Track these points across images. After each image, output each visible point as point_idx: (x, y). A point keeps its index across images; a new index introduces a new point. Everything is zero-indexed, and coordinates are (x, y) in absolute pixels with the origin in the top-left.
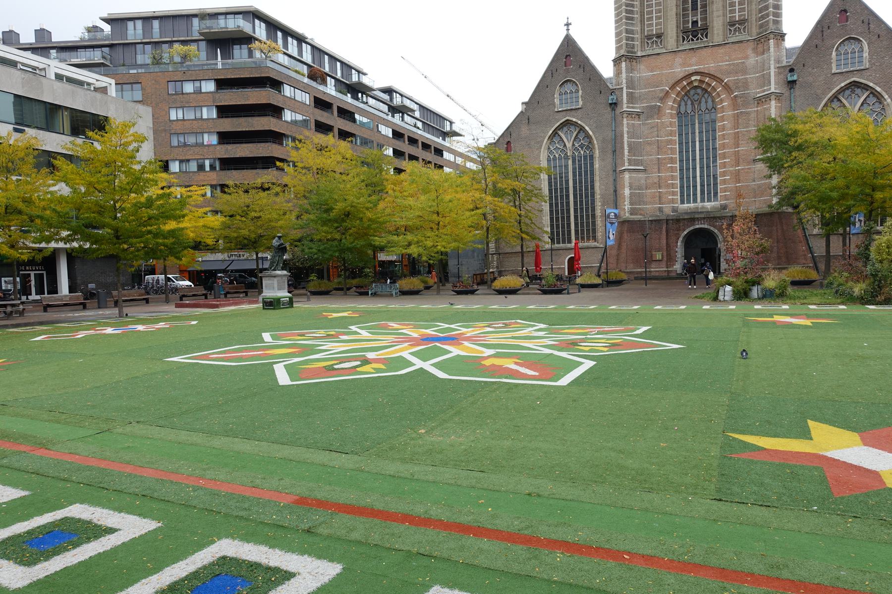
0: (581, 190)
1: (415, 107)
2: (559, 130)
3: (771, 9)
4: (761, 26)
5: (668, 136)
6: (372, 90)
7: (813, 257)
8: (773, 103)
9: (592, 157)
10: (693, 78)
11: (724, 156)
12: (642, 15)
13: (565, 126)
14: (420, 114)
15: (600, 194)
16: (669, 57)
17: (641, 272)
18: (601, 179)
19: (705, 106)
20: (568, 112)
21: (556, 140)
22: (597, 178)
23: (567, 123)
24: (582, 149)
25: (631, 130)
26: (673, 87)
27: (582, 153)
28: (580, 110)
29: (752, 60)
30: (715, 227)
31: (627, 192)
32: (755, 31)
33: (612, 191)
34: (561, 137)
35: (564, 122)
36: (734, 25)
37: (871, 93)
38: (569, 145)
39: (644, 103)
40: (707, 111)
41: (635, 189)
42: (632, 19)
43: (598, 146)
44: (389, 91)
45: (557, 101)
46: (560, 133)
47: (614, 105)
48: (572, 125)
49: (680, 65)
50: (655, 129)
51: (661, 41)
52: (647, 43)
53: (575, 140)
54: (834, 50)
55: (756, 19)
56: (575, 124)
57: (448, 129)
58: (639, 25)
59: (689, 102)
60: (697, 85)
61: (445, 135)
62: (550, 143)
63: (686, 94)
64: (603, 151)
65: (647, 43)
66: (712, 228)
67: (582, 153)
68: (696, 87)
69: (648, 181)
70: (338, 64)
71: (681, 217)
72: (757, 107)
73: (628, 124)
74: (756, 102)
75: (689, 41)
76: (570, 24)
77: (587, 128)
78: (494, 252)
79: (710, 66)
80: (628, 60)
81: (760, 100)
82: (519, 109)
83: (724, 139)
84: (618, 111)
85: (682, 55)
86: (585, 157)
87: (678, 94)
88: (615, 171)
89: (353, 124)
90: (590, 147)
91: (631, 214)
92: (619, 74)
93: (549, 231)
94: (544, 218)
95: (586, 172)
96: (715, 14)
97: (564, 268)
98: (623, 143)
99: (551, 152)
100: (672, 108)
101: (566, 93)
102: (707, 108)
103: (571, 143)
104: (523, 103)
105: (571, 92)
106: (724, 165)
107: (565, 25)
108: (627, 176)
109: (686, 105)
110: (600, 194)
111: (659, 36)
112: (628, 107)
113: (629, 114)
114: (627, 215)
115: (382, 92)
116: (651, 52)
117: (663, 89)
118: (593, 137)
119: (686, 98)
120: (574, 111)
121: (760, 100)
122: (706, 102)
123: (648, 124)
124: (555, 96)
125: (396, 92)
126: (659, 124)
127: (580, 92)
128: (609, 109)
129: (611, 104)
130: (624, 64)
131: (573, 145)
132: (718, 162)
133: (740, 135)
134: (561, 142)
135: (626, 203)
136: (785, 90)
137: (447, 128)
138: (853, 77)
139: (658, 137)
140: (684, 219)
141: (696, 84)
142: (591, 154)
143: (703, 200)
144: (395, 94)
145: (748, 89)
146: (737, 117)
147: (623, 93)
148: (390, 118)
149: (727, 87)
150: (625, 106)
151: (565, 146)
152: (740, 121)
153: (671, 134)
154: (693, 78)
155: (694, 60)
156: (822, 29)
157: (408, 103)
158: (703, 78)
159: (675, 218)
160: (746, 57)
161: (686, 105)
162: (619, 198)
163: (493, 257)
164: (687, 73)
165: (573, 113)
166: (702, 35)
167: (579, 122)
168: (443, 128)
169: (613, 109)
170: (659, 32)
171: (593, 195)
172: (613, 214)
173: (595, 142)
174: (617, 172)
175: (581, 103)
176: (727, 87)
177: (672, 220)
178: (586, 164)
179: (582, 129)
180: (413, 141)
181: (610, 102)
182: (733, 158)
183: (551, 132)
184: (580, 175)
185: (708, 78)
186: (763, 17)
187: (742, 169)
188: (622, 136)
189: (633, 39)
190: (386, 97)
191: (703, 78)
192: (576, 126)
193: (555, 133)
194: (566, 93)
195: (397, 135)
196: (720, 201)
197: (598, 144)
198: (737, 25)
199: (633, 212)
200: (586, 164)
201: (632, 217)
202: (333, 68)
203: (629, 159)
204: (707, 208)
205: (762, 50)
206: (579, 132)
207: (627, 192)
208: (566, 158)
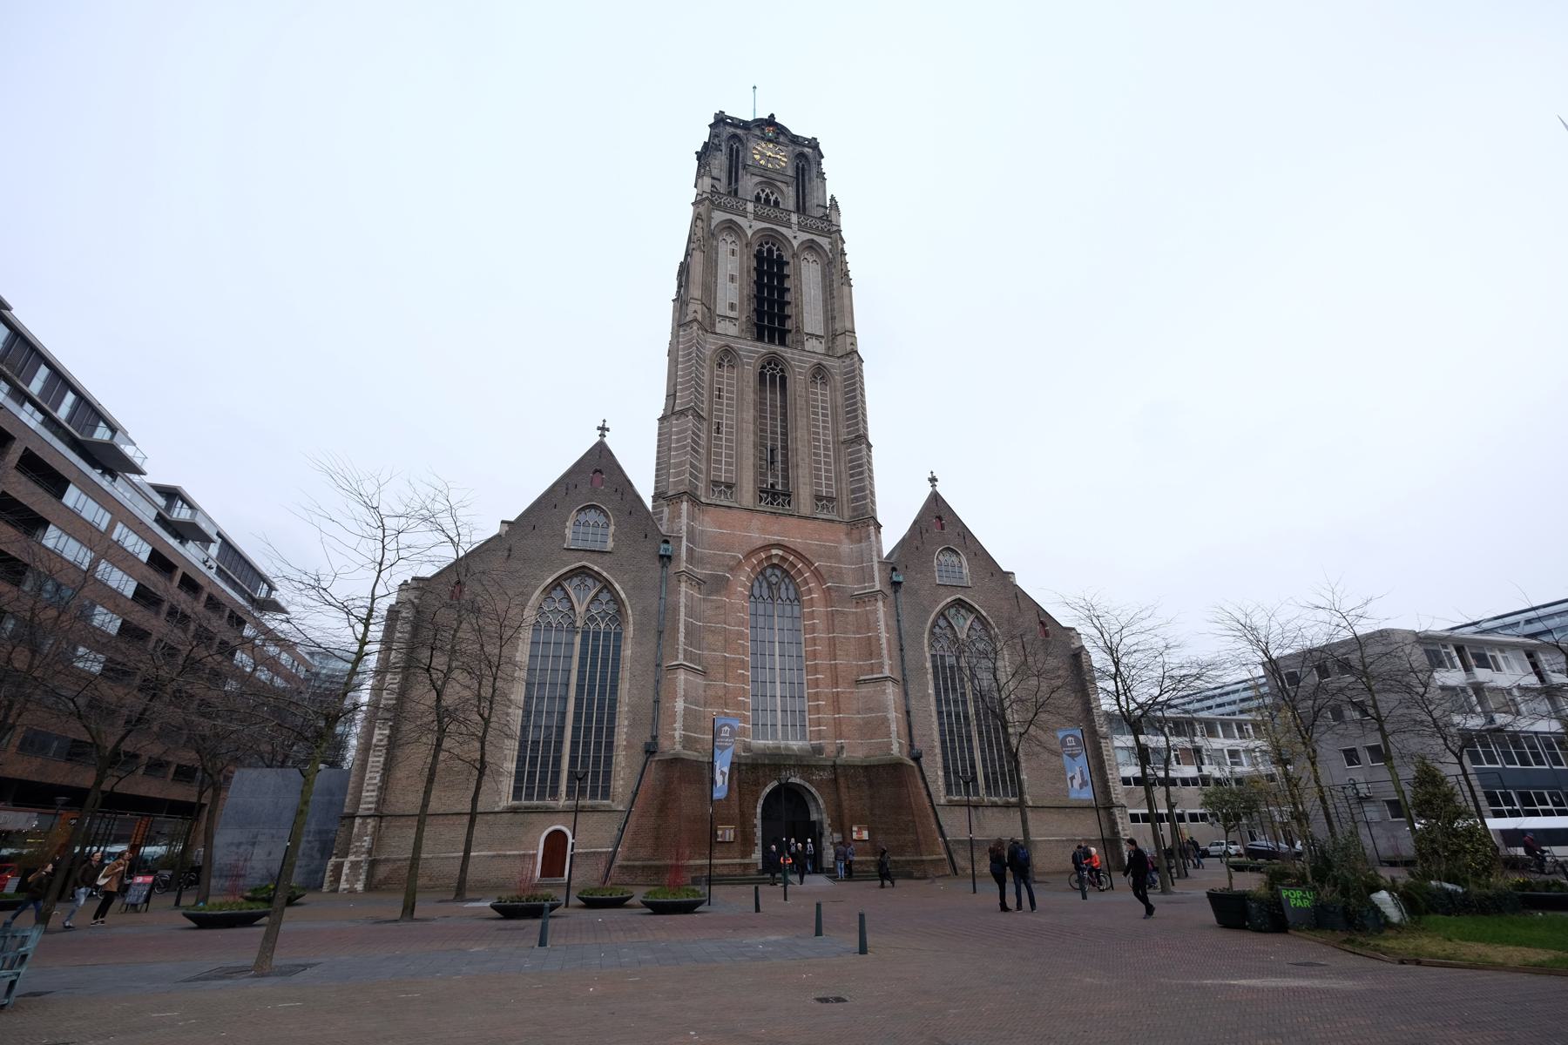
0: (591, 692)
2: (565, 580)
4: (855, 509)
5: (739, 626)
7: (946, 842)
9: (618, 636)
10: (774, 552)
13: (576, 576)
14: (219, 554)
15: (628, 705)
16: (745, 515)
17: (701, 867)
18: (633, 676)
19: (785, 594)
20: (588, 554)
21: (558, 594)
22: (625, 675)
23: (583, 572)
24: (603, 620)
25: (690, 604)
26: (748, 556)
27: (602, 626)
28: (606, 557)
29: (846, 547)
30: (811, 782)
31: (680, 705)
32: (847, 514)
33: (651, 701)
34: (566, 593)
35: (576, 569)
36: (821, 500)
37: (977, 617)
39: (707, 569)
40: (788, 602)
41: (691, 703)
43: (634, 619)
44: (172, 494)
45: (569, 533)
46: (566, 585)
47: (666, 559)
48: (590, 576)
50: (722, 611)
51: (732, 493)
52: (713, 490)
53: (592, 602)
55: (848, 501)
56: (596, 576)
57: (263, 595)
59: (765, 585)
60: (777, 562)
62: (545, 600)
63: (761, 572)
64: (640, 628)
65: (713, 490)
66: (807, 785)
67: (602, 626)
68: (774, 566)
69: (709, 692)
71: (760, 761)
72: (856, 607)
74: (854, 601)
75: (767, 504)
77: (617, 586)
78: (372, 812)
79: (795, 540)
80: (690, 502)
81: (860, 598)
82: (494, 529)
83: (815, 645)
84: (672, 569)
85: (761, 517)
86: (607, 635)
87: (753, 569)
88: (658, 665)
89: (54, 500)
90: (619, 615)
91: (684, 747)
92: (674, 518)
93: (514, 771)
95: (605, 661)
96: (801, 480)
97: (535, 856)
98: (676, 621)
100: (744, 586)
101: (586, 524)
102: (788, 598)
104: (503, 522)
105: (596, 525)
107: (599, 428)
108: (682, 676)
109: (761, 587)
110: (628, 705)
111: (729, 486)
113: (689, 578)
114: (678, 747)
115: (158, 492)
116: (718, 502)
117: (735, 556)
118: (627, 603)
119: (760, 578)
120: (596, 555)
121: (860, 598)
122: (787, 589)
123: (712, 601)
124: (568, 524)
126: (727, 605)
127: (612, 528)
128: (657, 563)
129: (662, 557)
131: (588, 610)
133: (837, 642)
134: (565, 601)
136: (888, 591)
137: (262, 592)
139: (725, 624)
140: (764, 765)
141: (775, 561)
142: (618, 630)
143: (785, 737)
144: (180, 503)
145: (843, 582)
146: (831, 616)
147: (681, 544)
149: (817, 574)
151: (572, 608)
152: (836, 622)
153: (742, 623)
154: (774, 552)
155: (776, 528)
156: (918, 527)
158: (786, 555)
159: (749, 761)
160: (840, 542)
161: (761, 587)
162: (662, 715)
163: (364, 824)
164: (767, 543)
165: (595, 556)
167: (605, 574)
168: (255, 590)
170: (728, 481)
171: (613, 706)
172: (726, 728)
173: (629, 612)
176: (817, 574)
177: (746, 764)
178: (606, 647)
179: (607, 586)
181: (662, 552)
182: (828, 674)
183: (550, 580)
184: (594, 665)
185: (792, 557)
186: (857, 499)
187: (843, 693)
188: (676, 610)
189: (696, 478)
190: (161, 501)
191: (786, 555)
192: (595, 578)
193: (557, 584)
194: (586, 524)
195: (160, 562)
196: (810, 740)
197: (633, 615)
198: (825, 502)
199: (688, 742)
200: (606, 647)
201: (686, 752)
203: (685, 650)
204: (793, 750)
205: (858, 538)
206: (600, 591)
207: (680, 705)
208: (573, 629)
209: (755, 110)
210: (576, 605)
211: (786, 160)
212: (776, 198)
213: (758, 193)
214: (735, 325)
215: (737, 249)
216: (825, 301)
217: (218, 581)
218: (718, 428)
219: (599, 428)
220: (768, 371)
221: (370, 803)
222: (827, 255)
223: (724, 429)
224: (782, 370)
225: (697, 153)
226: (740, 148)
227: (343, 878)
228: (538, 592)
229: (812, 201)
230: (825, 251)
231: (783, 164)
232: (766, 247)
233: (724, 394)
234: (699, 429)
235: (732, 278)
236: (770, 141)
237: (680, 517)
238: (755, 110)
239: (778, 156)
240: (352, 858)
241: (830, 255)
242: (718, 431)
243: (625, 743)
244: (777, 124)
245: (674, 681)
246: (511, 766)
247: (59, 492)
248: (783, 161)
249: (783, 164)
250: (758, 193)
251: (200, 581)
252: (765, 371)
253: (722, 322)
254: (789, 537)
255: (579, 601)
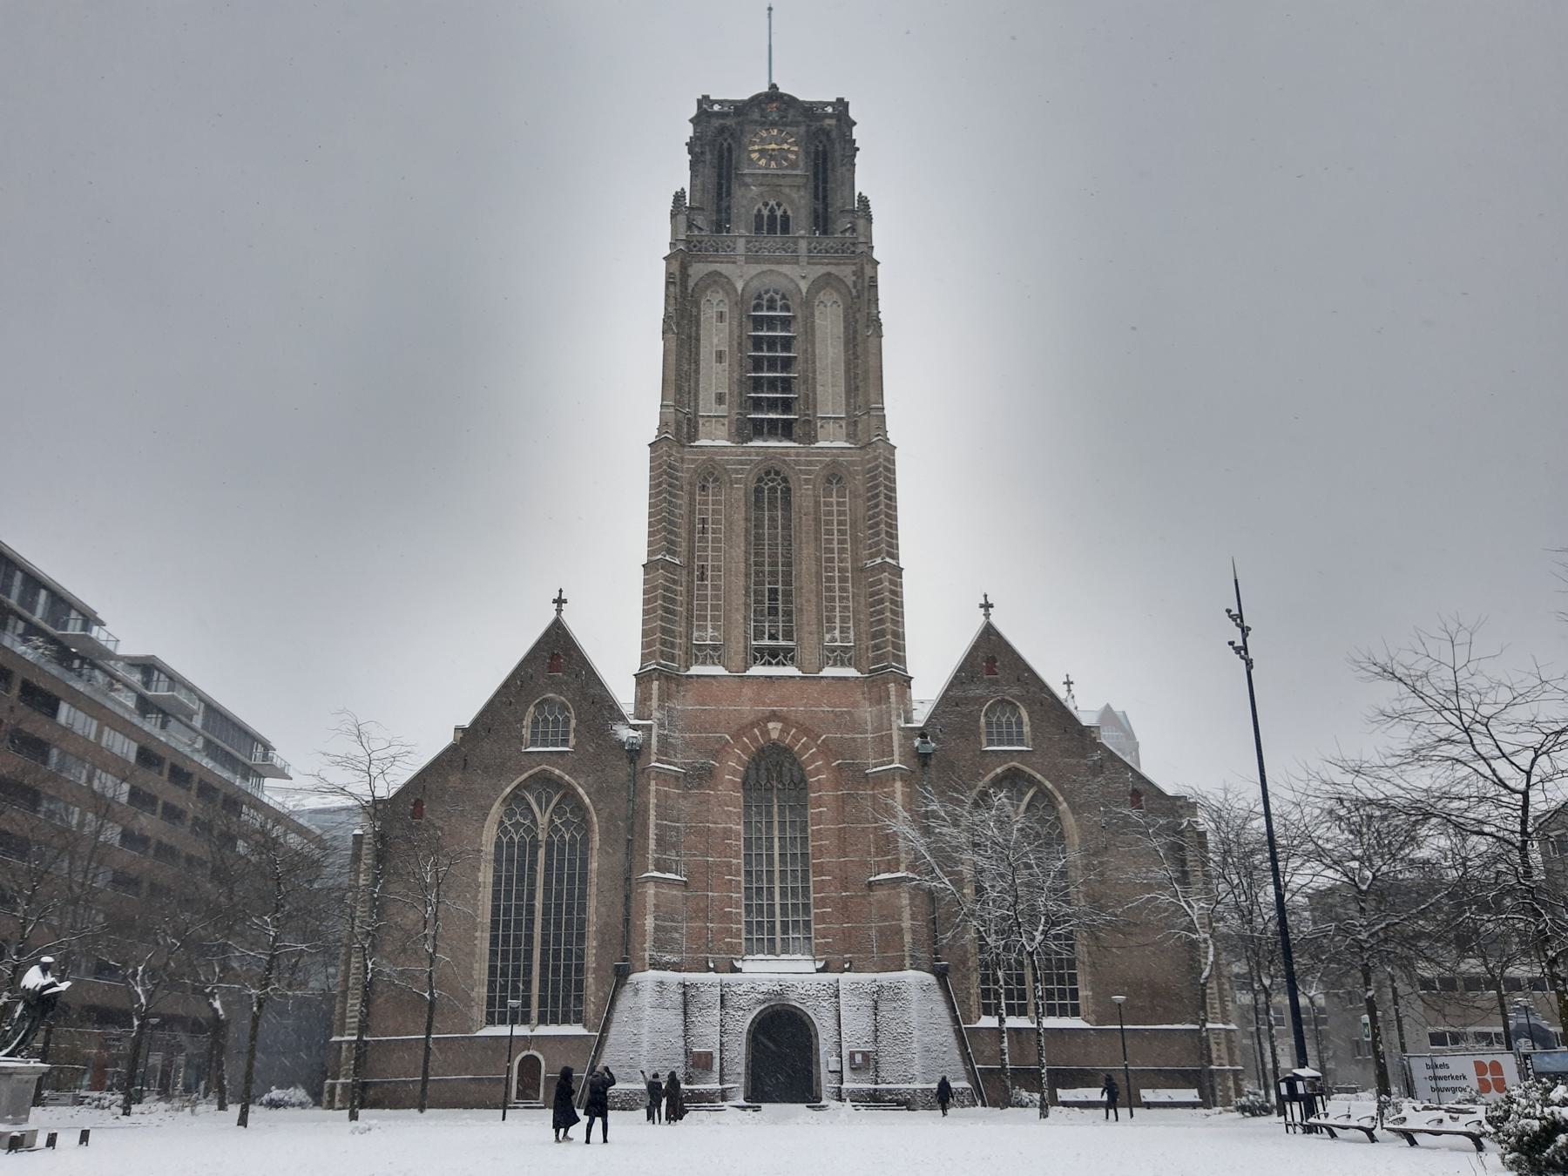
1: (195, 706)
3: (889, 637)
6: (110, 655)
8: (898, 785)
11: (820, 871)
12: (690, 610)
22: (592, 890)
24: (568, 830)
31: (650, 923)
38: (543, 820)
42: (673, 612)
44: (148, 667)
49: (750, 700)
54: (983, 714)
58: (684, 624)
61: (248, 772)
64: (605, 833)
70: (43, 594)
73: (657, 791)
76: (565, 601)
80: (663, 681)
82: (446, 739)
90: (584, 825)
94: (476, 966)
98: (645, 826)
99: (505, 831)
100: (734, 772)
103: (547, 815)
106: (821, 887)
107: (982, 606)
112: (658, 761)
118: (592, 809)
124: (525, 723)
125: (160, 671)
130: (655, 685)
131: (551, 821)
132: (812, 879)
135: (647, 945)
138: (1012, 761)
148: (136, 720)
150: (654, 758)
151: (534, 821)
157: (182, 696)
160: (855, 704)
162: (632, 935)
166: (785, 657)
169: (632, 761)
173: (595, 819)
174: (633, 882)
175: (572, 741)
180: (180, 775)
183: (508, 790)
188: (647, 810)
195: (148, 757)
198: (839, 652)
202: (28, 601)
207: (650, 923)
209: (770, 46)
210: (538, 815)
211: (796, 149)
212: (785, 212)
213: (759, 210)
214: (724, 425)
215: (726, 309)
216: (848, 363)
217: (207, 763)
218: (703, 573)
219: (555, 601)
220: (766, 484)
221: (353, 1029)
222: (850, 292)
223: (709, 573)
224: (785, 480)
225: (687, 144)
226: (733, 145)
227: (337, 1098)
228: (497, 804)
229: (837, 202)
230: (847, 286)
231: (792, 157)
232: (766, 297)
233: (710, 526)
234: (675, 582)
235: (720, 356)
236: (773, 124)
237: (651, 699)
238: (770, 46)
239: (786, 146)
240: (342, 1080)
241: (854, 291)
242: (702, 578)
243: (594, 965)
244: (783, 95)
245: (644, 894)
246: (590, 979)
247: (53, 711)
248: (792, 152)
249: (792, 157)
250: (759, 210)
251: (188, 768)
252: (762, 484)
253: (707, 424)
254: (788, 706)
255: (541, 809)
